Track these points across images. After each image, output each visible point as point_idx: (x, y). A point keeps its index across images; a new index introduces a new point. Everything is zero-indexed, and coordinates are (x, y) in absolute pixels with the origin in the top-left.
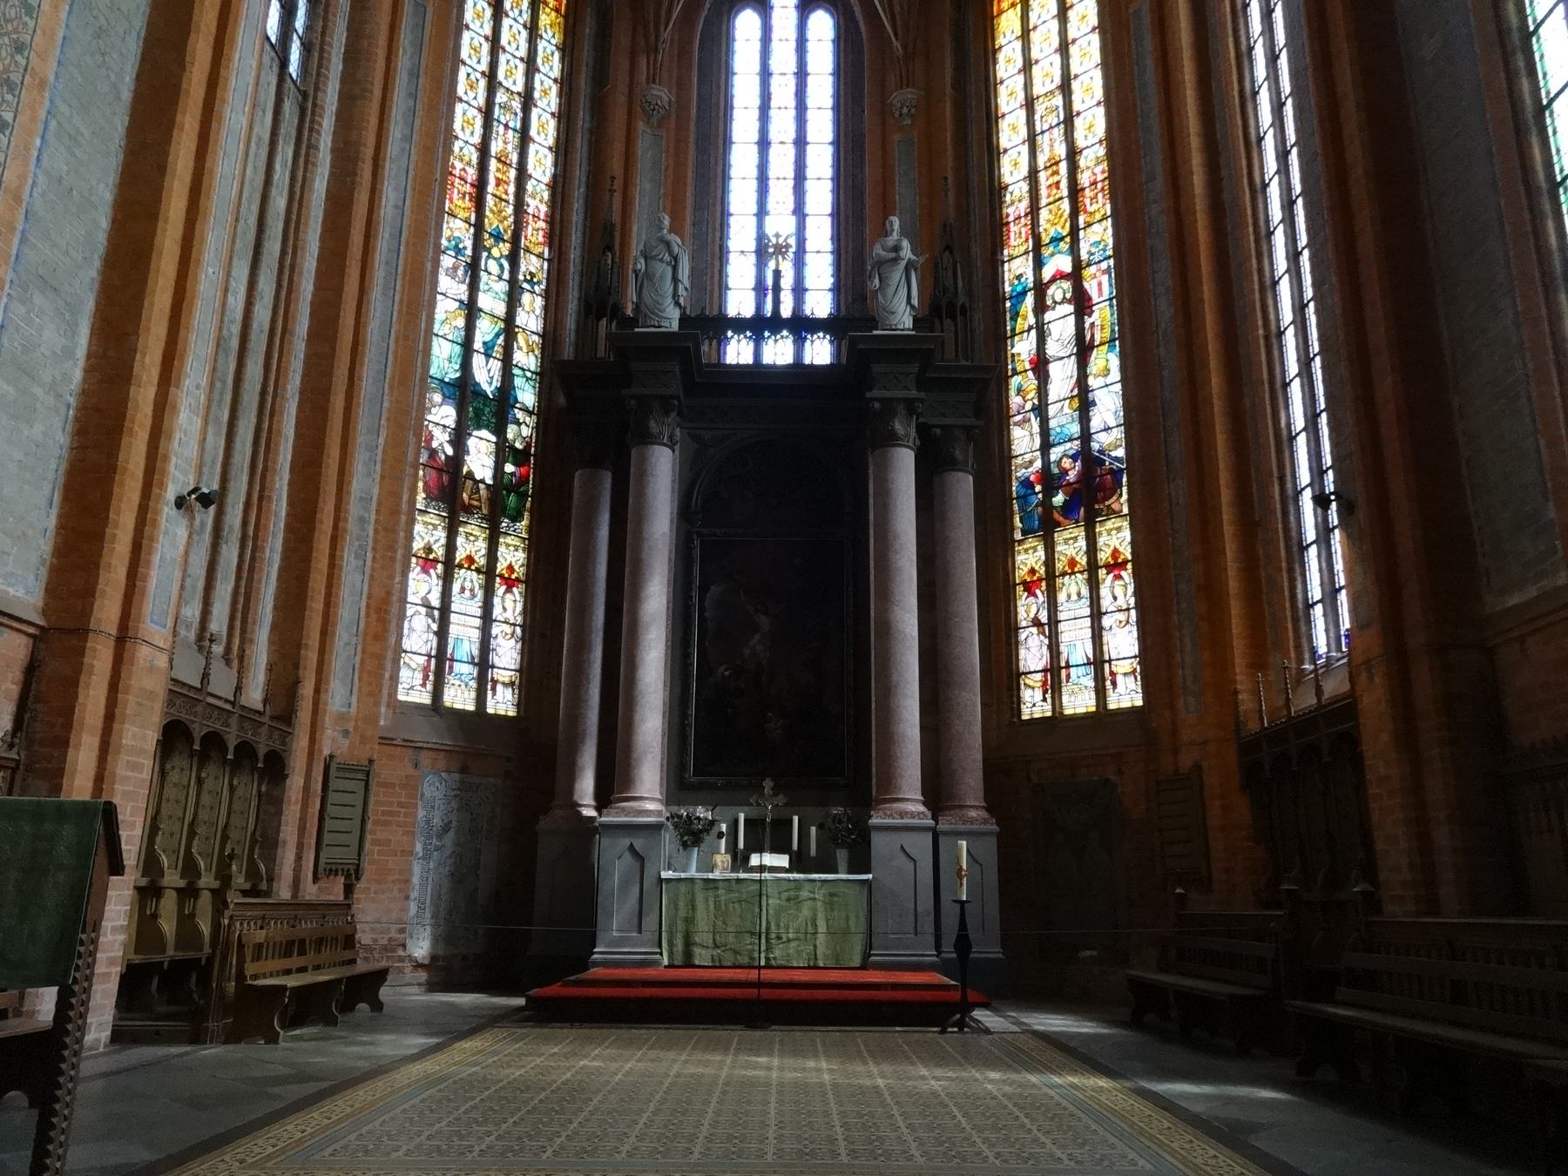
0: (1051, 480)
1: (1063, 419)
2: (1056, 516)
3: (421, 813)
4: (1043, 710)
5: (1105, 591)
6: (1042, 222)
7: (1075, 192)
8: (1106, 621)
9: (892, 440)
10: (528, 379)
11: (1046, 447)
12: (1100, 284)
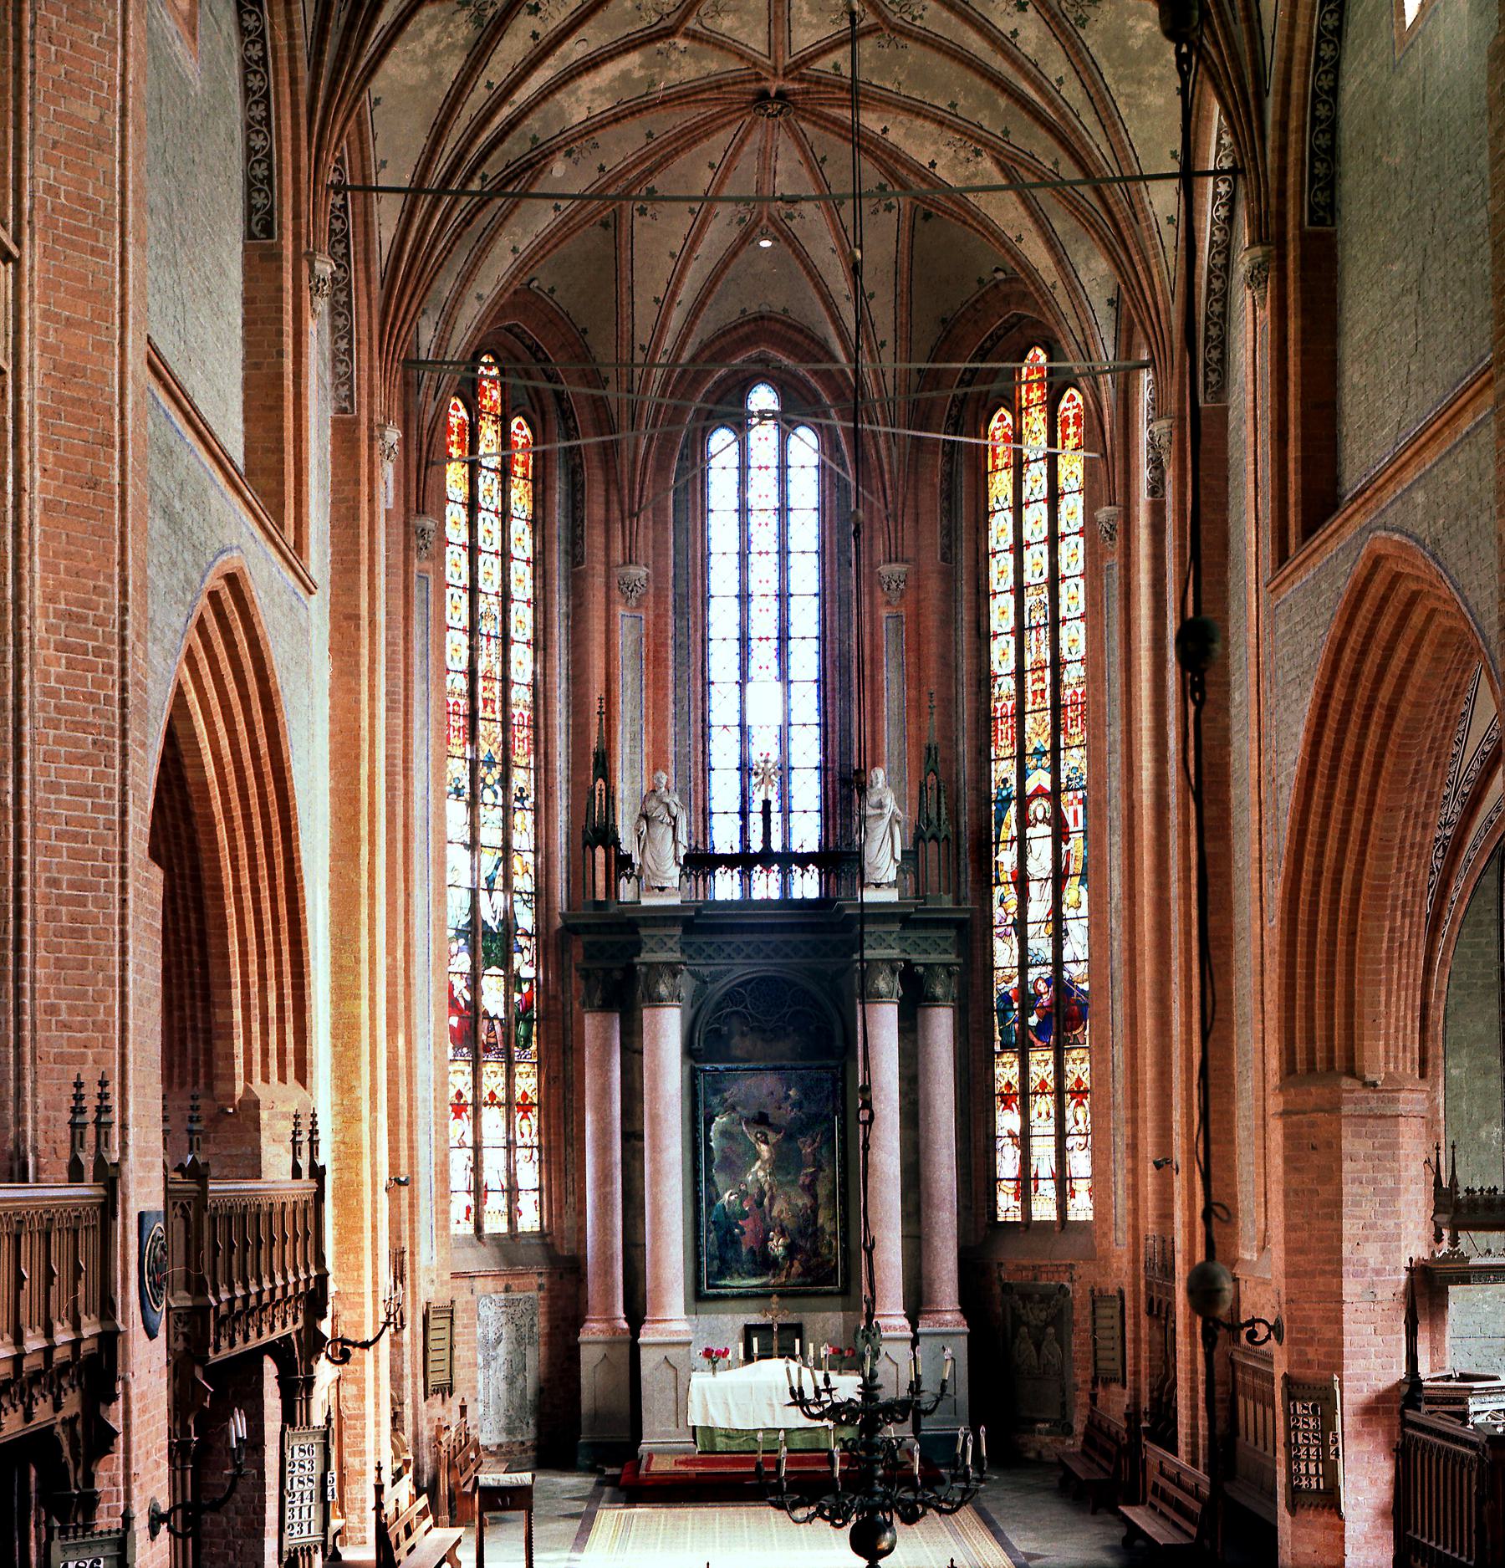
1: (1040, 945)
3: (479, 1331)
4: (1015, 1216)
6: (1027, 729)
8: (1070, 1142)
9: (871, 996)
10: (525, 902)
11: (1024, 966)
12: (1076, 813)
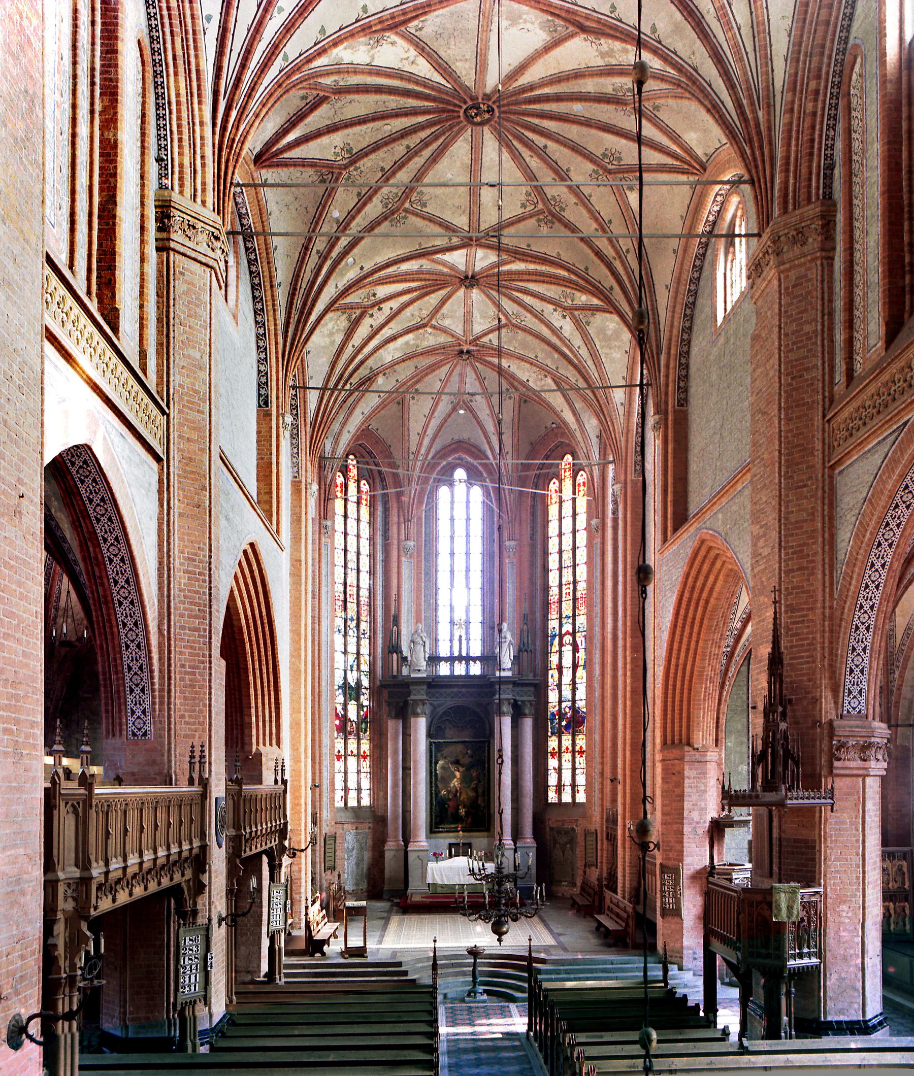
0: (561, 714)
1: (567, 693)
5: (577, 760)
7: (575, 600)
8: (577, 772)
9: (501, 714)
11: (560, 702)
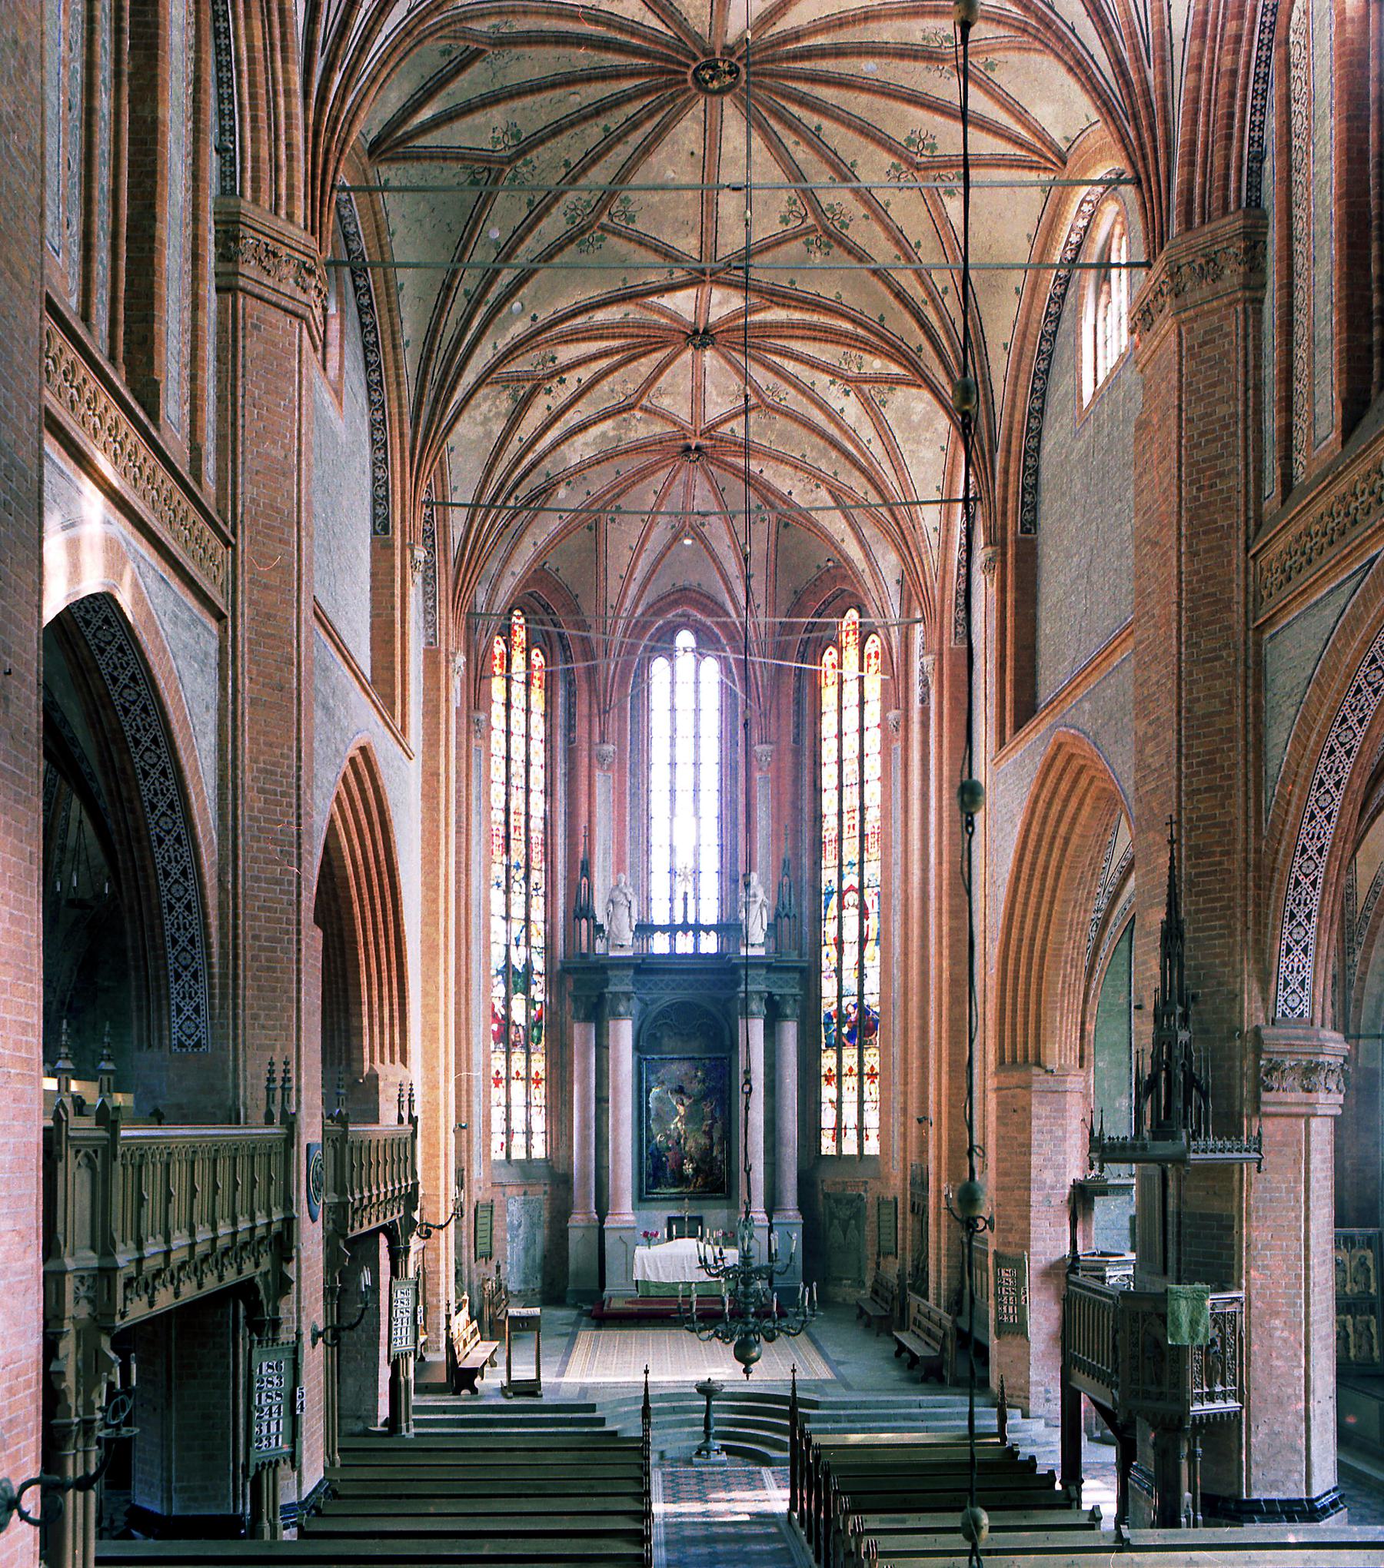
0: (841, 1017)
1: (850, 982)
2: (844, 1040)
7: (862, 836)
8: (866, 1106)
9: (748, 1014)
11: (840, 997)
